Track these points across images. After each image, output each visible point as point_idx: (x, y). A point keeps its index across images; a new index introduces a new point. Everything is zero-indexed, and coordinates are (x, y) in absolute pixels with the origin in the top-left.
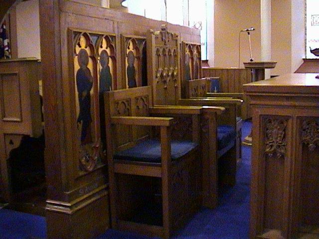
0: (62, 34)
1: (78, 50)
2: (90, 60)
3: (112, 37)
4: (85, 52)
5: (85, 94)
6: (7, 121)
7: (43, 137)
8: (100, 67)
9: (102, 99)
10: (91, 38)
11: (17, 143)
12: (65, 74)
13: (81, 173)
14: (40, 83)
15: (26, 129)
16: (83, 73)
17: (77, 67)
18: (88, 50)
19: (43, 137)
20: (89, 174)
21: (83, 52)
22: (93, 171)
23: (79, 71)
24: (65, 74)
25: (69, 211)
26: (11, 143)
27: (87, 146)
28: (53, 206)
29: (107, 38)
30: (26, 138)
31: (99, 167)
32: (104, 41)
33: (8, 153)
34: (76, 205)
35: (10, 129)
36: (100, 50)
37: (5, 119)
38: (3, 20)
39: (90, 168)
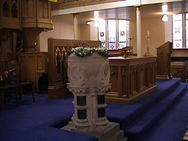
0: (121, 84)
1: (57, 51)
2: (60, 53)
3: (67, 47)
4: (58, 51)
5: (58, 61)
6: (39, 69)
7: (48, 74)
8: (62, 55)
9: (63, 63)
10: (60, 47)
11: (41, 76)
12: (53, 56)
13: (57, 80)
14: (48, 59)
15: (44, 71)
16: (58, 56)
17: (56, 55)
18: (59, 51)
19: (48, 74)
20: (59, 81)
21: (58, 51)
22: (60, 81)
23: (57, 56)
24: (53, 56)
25: (53, 89)
26: (39, 75)
27: (59, 74)
28: (50, 88)
29: (65, 47)
30: (43, 74)
31: (62, 80)
32: (64, 48)
33: (38, 78)
34: (55, 87)
35: (39, 71)
36: (63, 50)
37: (38, 68)
38: (144, 57)
39: (59, 80)
